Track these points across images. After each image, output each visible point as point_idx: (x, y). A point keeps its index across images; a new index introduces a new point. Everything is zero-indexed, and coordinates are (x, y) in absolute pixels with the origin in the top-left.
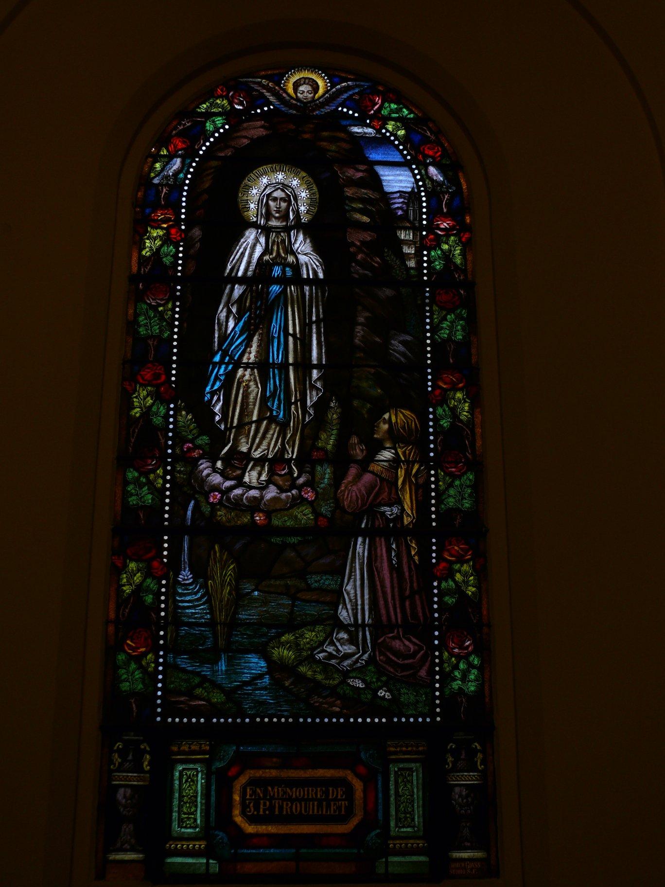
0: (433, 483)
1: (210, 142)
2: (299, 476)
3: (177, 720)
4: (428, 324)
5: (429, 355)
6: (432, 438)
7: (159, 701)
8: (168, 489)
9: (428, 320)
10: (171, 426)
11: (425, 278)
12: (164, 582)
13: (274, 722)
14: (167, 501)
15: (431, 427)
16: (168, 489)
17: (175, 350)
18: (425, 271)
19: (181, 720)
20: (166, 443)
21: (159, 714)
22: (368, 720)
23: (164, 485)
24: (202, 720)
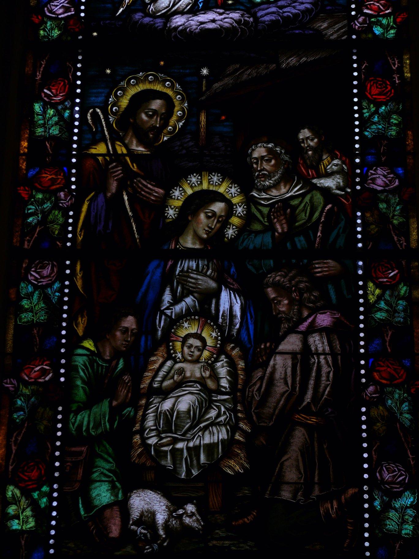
0: (366, 501)
1: (359, 225)
2: (353, 24)
3: (367, 525)
4: (357, 119)
5: (364, 427)
6: (355, 65)
7: (52, 541)
8: (65, 303)
9: (361, 301)
10: (70, 236)
11: (368, 554)
12: (67, 283)
13: (360, 248)
14: (75, 138)
15: (362, 347)
16: (65, 303)
17: (65, 316)
18: (362, 326)
19: (366, 520)
20: (61, 298)
21: (55, 509)
22: (367, 544)
23: (61, 298)
24: (360, 245)
